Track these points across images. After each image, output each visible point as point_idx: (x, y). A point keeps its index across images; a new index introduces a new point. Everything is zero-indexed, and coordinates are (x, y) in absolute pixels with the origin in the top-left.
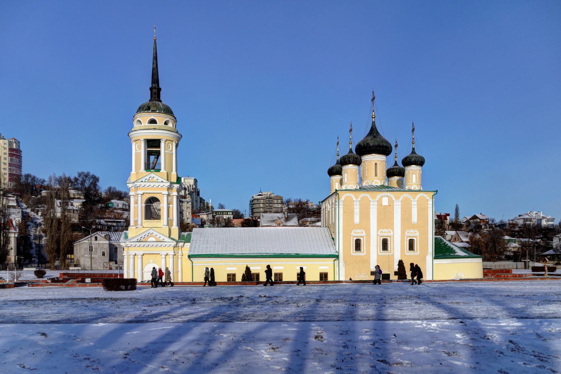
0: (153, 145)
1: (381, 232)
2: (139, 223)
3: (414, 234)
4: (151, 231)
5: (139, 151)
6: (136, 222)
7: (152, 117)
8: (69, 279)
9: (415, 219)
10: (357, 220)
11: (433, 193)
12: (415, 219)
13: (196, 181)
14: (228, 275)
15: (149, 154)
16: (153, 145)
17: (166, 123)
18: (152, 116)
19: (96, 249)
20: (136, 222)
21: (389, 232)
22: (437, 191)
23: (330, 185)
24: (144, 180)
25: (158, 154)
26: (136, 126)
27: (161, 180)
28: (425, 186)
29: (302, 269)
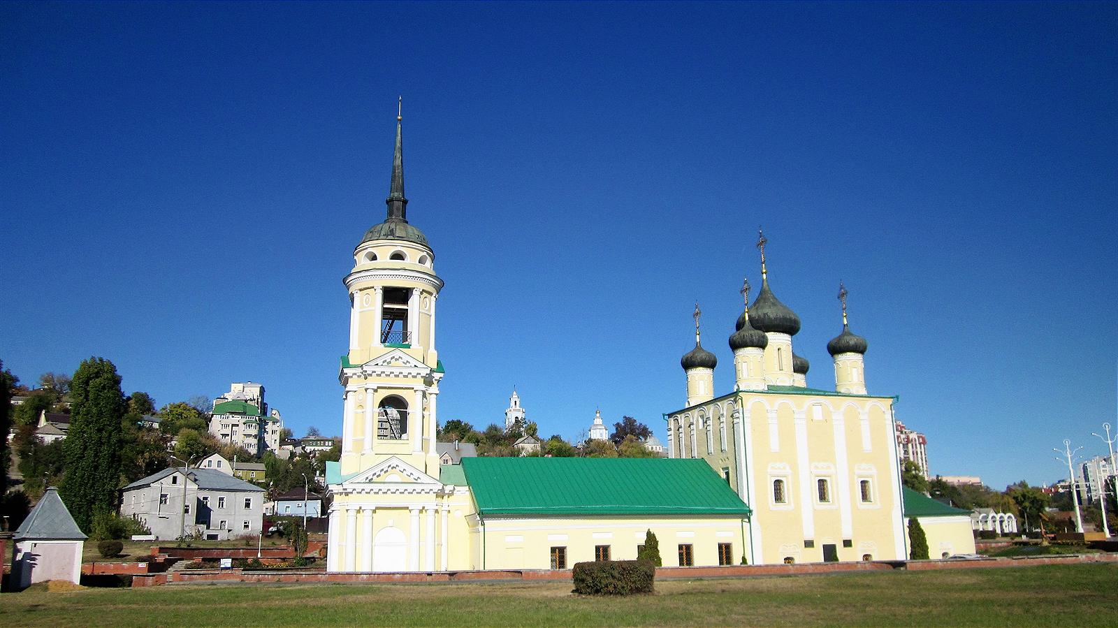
0: (396, 296)
1: (816, 467)
2: (367, 445)
3: (867, 471)
4: (394, 462)
5: (367, 312)
6: (359, 443)
7: (399, 248)
8: (176, 561)
9: (867, 445)
10: (774, 444)
11: (890, 401)
12: (867, 445)
13: (262, 391)
14: (597, 548)
15: (387, 313)
16: (396, 296)
17: (421, 261)
18: (399, 246)
19: (173, 498)
20: (359, 443)
21: (829, 467)
22: (897, 397)
23: (685, 389)
24: (380, 363)
25: (403, 315)
26: (362, 261)
27: (413, 363)
28: (875, 388)
29: (649, 534)
